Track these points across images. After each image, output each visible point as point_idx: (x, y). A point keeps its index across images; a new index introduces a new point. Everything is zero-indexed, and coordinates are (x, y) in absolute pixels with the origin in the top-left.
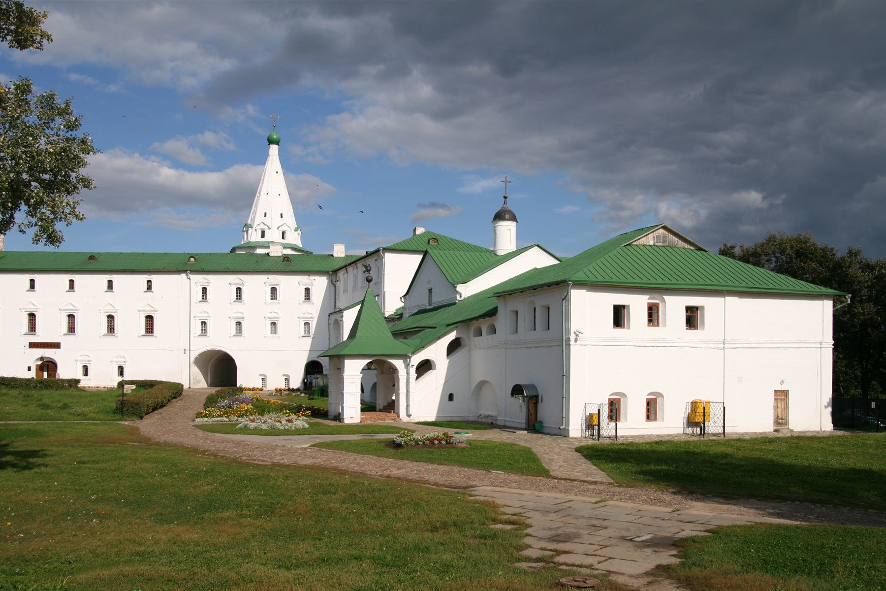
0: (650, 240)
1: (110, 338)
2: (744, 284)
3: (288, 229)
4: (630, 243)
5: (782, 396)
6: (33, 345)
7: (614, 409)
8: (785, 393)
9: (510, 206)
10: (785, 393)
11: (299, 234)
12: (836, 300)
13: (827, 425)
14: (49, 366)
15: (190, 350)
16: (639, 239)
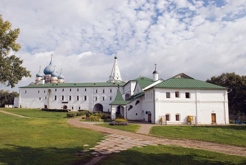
5: (214, 115)
6: (63, 103)
8: (215, 114)
10: (215, 114)
14: (66, 107)
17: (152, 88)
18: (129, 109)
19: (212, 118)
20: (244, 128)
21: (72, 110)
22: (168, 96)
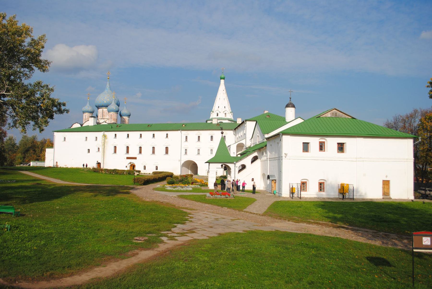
0: (329, 115)
1: (153, 155)
2: (367, 133)
3: (227, 112)
4: (320, 116)
5: (386, 183)
6: (128, 158)
7: (304, 185)
9: (293, 102)
11: (232, 114)
12: (415, 139)
13: (412, 197)
14: (133, 166)
15: (181, 160)
16: (324, 114)
17: (278, 135)
18: (240, 171)
19: (383, 188)
20: (1, 182)
21: (143, 171)
22: (306, 147)
